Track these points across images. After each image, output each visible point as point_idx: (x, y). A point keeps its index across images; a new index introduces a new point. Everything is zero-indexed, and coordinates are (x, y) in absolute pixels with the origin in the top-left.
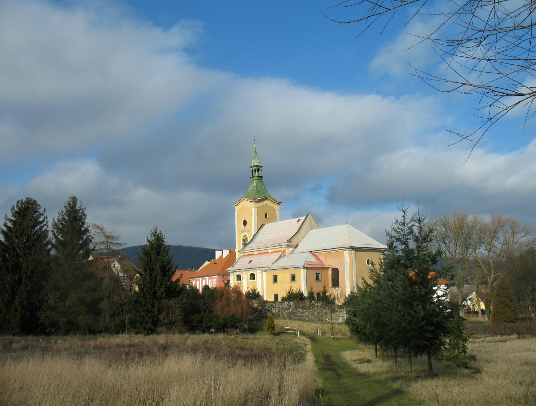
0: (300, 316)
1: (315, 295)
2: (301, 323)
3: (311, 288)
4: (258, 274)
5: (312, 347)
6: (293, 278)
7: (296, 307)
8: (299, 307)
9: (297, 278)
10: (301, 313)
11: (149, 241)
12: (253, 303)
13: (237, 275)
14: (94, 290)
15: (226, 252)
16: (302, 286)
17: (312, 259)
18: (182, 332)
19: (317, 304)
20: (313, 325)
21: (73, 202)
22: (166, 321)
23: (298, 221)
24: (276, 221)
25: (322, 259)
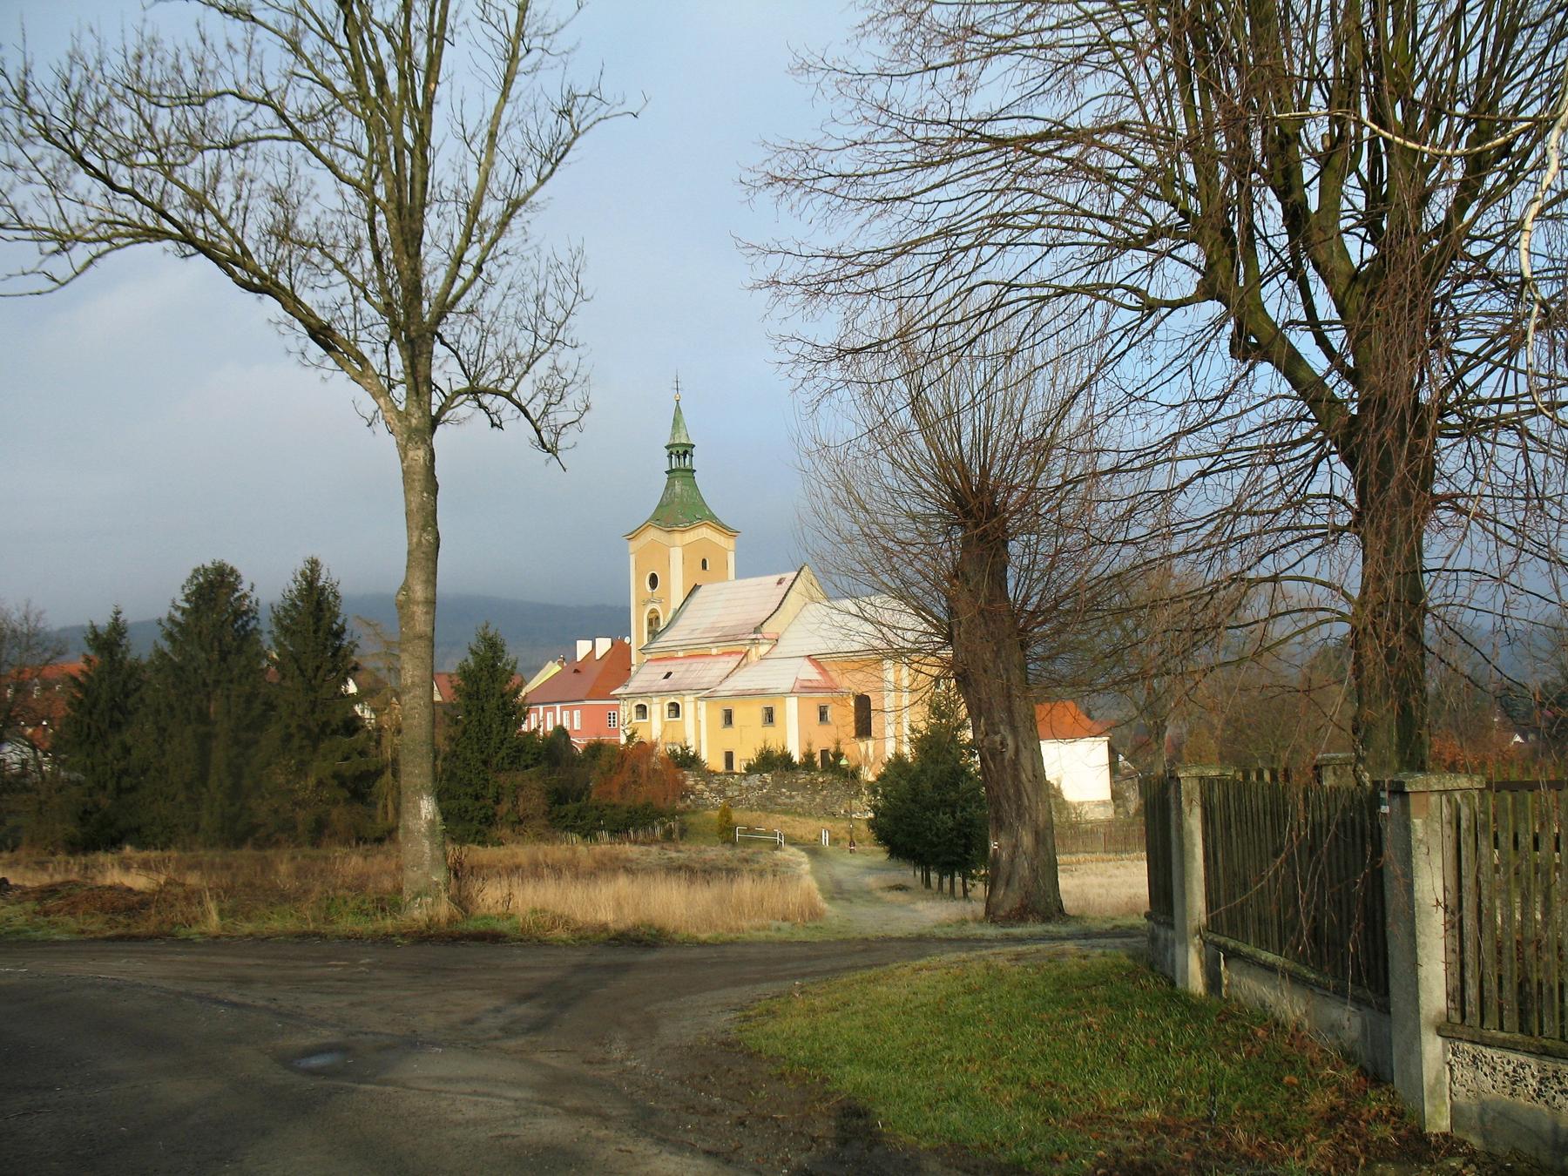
1: (818, 758)
2: (786, 818)
3: (809, 745)
6: (769, 716)
7: (777, 786)
9: (776, 716)
11: (474, 653)
14: (362, 753)
15: (604, 645)
16: (792, 739)
20: (812, 823)
22: (513, 818)
23: (780, 582)
24: (726, 579)
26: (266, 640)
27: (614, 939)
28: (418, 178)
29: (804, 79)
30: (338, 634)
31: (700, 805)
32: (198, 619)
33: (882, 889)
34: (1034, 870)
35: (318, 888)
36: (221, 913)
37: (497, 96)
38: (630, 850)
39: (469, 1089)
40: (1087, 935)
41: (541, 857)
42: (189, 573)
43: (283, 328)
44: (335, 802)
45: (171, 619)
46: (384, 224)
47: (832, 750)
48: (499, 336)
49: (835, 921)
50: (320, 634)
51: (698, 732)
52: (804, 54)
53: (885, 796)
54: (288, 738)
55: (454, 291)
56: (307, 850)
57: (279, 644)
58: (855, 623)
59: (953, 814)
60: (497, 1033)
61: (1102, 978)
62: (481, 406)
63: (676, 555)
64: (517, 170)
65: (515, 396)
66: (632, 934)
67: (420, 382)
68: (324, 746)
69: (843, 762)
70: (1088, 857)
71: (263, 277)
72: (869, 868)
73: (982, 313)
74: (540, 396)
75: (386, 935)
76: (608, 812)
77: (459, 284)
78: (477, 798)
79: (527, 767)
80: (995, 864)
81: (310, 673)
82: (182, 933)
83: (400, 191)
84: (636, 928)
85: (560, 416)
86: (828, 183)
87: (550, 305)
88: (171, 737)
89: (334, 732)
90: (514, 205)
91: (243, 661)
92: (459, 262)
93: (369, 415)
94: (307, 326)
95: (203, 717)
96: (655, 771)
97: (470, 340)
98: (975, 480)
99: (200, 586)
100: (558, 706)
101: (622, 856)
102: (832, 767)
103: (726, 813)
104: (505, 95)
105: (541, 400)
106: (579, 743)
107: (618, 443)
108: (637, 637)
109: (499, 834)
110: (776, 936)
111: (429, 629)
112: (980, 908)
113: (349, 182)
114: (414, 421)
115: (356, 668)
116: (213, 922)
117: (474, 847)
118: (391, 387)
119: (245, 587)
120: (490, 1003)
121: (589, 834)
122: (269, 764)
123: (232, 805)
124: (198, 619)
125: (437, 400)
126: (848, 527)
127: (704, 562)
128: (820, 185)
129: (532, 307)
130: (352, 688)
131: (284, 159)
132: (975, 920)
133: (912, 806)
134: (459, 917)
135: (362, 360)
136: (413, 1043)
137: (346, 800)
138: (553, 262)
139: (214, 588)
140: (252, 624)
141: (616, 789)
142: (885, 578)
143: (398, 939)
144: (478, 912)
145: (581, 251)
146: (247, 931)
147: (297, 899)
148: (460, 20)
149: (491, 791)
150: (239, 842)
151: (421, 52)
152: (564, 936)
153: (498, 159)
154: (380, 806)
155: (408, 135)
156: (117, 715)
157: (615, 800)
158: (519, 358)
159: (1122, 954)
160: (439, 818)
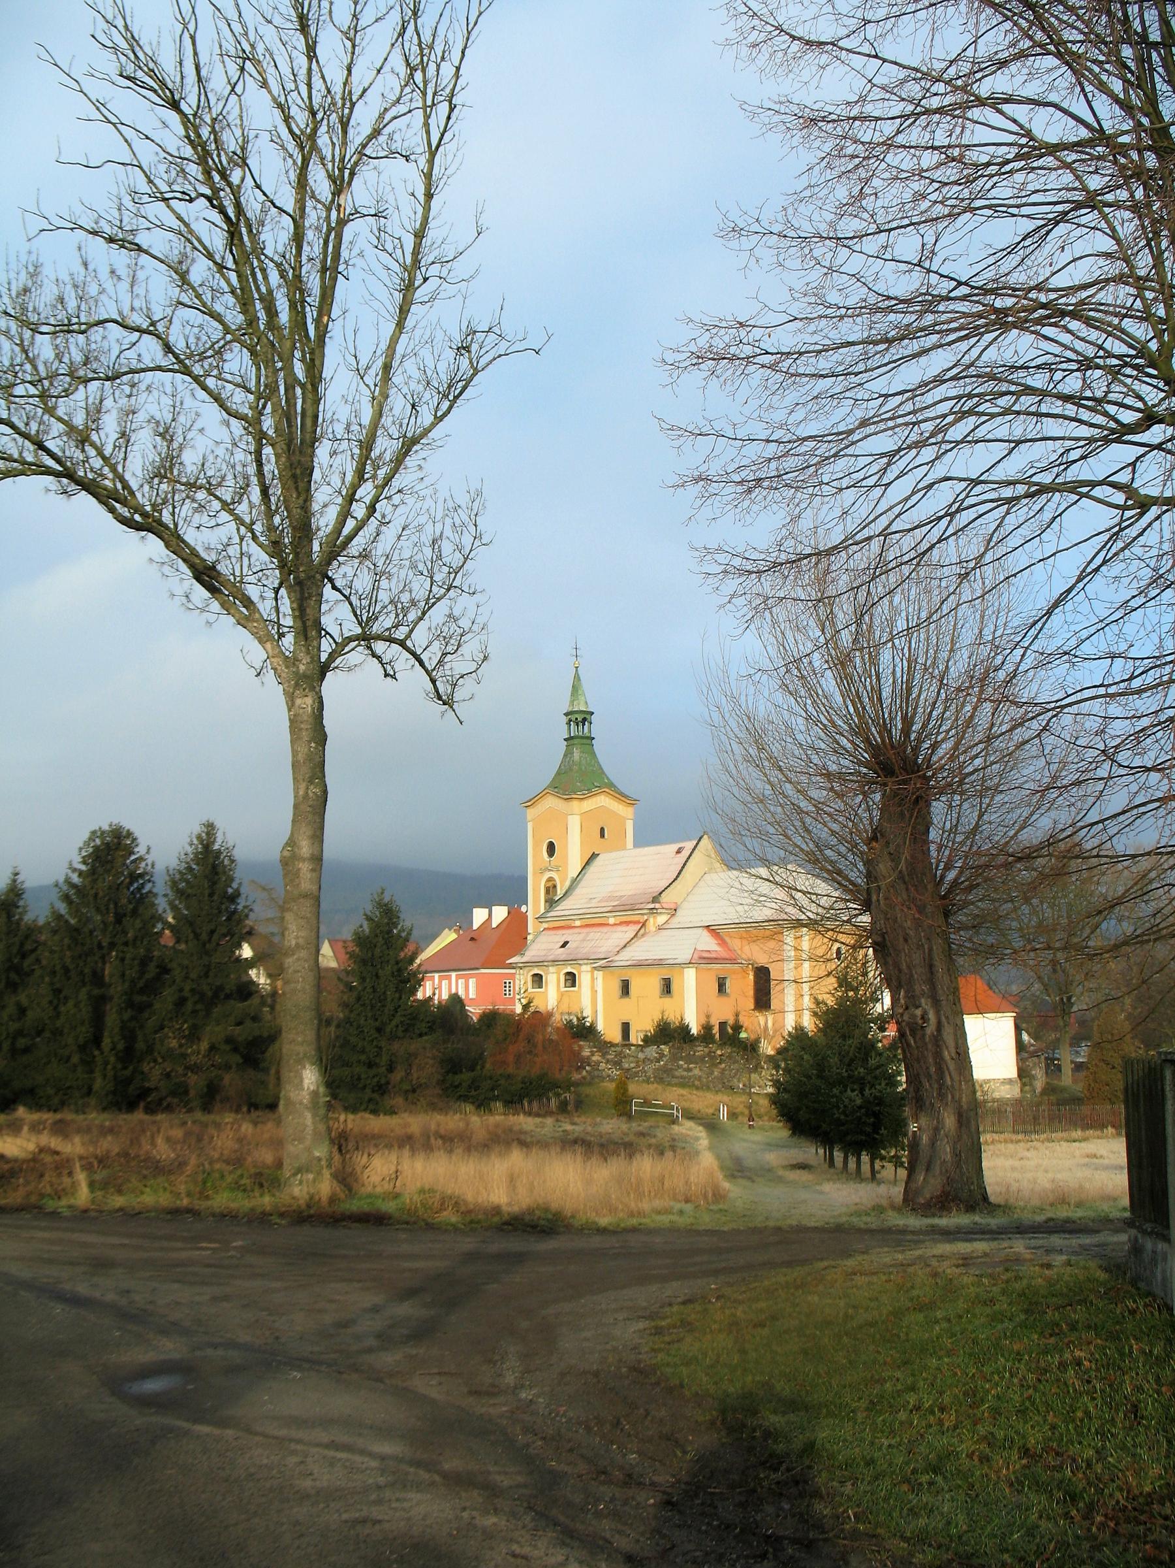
0: (682, 1077)
1: (716, 1030)
3: (708, 1017)
4: (584, 977)
5: (710, 1143)
6: (667, 987)
7: (674, 1058)
8: (682, 1058)
10: (685, 1070)
11: (369, 919)
12: (581, 1047)
13: (535, 975)
14: (255, 1019)
15: (500, 913)
17: (708, 944)
18: (426, 1111)
19: (719, 1052)
21: (208, 834)
22: (406, 1087)
23: (679, 852)
24: (624, 848)
25: (735, 944)
26: (162, 904)
27: (507, 1223)
28: (309, 413)
29: (734, 244)
30: (234, 898)
31: (596, 1077)
32: (95, 881)
33: (785, 1167)
34: (957, 1155)
35: (193, 1161)
36: (92, 1185)
37: (392, 326)
38: (524, 1122)
39: (325, 1437)
40: (1021, 1230)
41: (433, 1127)
42: (86, 836)
43: (166, 569)
44: (228, 1067)
45: (68, 881)
46: (273, 459)
47: (731, 1022)
48: (394, 580)
49: (739, 1203)
50: (215, 898)
51: (594, 1002)
52: (734, 215)
53: (787, 1071)
54: (181, 1002)
55: (346, 531)
56: (199, 1115)
57: (174, 908)
58: (765, 888)
59: (862, 1091)
60: (371, 1342)
61: (1075, 1295)
62: (374, 655)
63: (574, 823)
64: (413, 406)
65: (409, 643)
66: (527, 1218)
67: (309, 626)
68: (217, 1011)
69: (743, 1035)
70: (996, 1136)
71: (144, 515)
72: (769, 1144)
73: (940, 518)
74: (436, 644)
75: (264, 1213)
76: (502, 1082)
77: (350, 524)
78: (370, 1065)
79: (421, 1035)
80: (914, 1146)
81: (204, 936)
82: (51, 1205)
83: (290, 426)
84: (530, 1211)
85: (457, 665)
86: (766, 359)
87: (447, 548)
88: (66, 998)
89: (228, 997)
90: (409, 444)
91: (138, 923)
92: (351, 499)
93: (258, 665)
94: (192, 566)
95: (97, 979)
96: (551, 1041)
97: (363, 582)
98: (896, 733)
99: (96, 848)
100: (454, 974)
101: (516, 1128)
102: (730, 1040)
103: (622, 1086)
104: (400, 325)
105: (436, 648)
106: (474, 1011)
107: (513, 700)
108: (535, 905)
109: (393, 1102)
110: (682, 1221)
111: (315, 888)
112: (898, 1192)
113: (237, 416)
114: (302, 668)
115: (250, 933)
116: (83, 1195)
117: (367, 1115)
118: (281, 635)
119: (141, 850)
120: (370, 1299)
121: (482, 1104)
122: (162, 1028)
123: (125, 1068)
124: (95, 881)
125: (326, 646)
126: (760, 786)
127: (602, 830)
128: (758, 360)
129: (428, 552)
130: (247, 952)
131: (169, 390)
132: (893, 1207)
133: (818, 1082)
134: (342, 1196)
135: (248, 603)
136: (270, 1361)
137: (238, 1064)
138: (450, 504)
139: (111, 852)
140: (148, 887)
141: (511, 1059)
142: (798, 840)
143: (275, 1219)
144: (364, 1191)
145: (479, 493)
146: (118, 1205)
147: (170, 1172)
148: (355, 252)
149: (384, 1060)
150: (131, 1106)
151: (313, 282)
152: (454, 1219)
153: (393, 391)
154: (273, 1071)
155: (299, 370)
156: (13, 976)
157: (511, 1070)
158: (413, 603)
159: (1092, 1264)
160: (322, 1090)
